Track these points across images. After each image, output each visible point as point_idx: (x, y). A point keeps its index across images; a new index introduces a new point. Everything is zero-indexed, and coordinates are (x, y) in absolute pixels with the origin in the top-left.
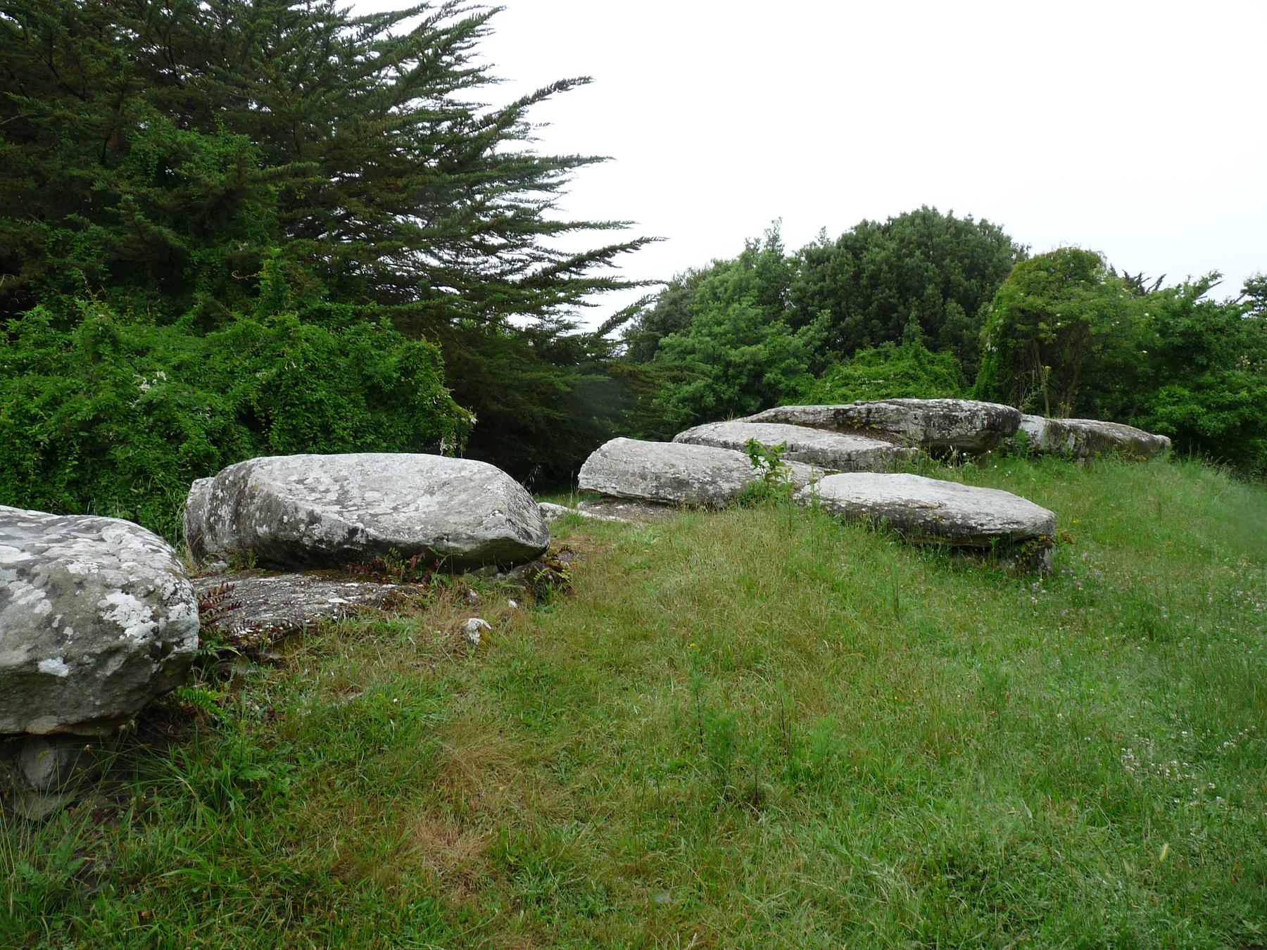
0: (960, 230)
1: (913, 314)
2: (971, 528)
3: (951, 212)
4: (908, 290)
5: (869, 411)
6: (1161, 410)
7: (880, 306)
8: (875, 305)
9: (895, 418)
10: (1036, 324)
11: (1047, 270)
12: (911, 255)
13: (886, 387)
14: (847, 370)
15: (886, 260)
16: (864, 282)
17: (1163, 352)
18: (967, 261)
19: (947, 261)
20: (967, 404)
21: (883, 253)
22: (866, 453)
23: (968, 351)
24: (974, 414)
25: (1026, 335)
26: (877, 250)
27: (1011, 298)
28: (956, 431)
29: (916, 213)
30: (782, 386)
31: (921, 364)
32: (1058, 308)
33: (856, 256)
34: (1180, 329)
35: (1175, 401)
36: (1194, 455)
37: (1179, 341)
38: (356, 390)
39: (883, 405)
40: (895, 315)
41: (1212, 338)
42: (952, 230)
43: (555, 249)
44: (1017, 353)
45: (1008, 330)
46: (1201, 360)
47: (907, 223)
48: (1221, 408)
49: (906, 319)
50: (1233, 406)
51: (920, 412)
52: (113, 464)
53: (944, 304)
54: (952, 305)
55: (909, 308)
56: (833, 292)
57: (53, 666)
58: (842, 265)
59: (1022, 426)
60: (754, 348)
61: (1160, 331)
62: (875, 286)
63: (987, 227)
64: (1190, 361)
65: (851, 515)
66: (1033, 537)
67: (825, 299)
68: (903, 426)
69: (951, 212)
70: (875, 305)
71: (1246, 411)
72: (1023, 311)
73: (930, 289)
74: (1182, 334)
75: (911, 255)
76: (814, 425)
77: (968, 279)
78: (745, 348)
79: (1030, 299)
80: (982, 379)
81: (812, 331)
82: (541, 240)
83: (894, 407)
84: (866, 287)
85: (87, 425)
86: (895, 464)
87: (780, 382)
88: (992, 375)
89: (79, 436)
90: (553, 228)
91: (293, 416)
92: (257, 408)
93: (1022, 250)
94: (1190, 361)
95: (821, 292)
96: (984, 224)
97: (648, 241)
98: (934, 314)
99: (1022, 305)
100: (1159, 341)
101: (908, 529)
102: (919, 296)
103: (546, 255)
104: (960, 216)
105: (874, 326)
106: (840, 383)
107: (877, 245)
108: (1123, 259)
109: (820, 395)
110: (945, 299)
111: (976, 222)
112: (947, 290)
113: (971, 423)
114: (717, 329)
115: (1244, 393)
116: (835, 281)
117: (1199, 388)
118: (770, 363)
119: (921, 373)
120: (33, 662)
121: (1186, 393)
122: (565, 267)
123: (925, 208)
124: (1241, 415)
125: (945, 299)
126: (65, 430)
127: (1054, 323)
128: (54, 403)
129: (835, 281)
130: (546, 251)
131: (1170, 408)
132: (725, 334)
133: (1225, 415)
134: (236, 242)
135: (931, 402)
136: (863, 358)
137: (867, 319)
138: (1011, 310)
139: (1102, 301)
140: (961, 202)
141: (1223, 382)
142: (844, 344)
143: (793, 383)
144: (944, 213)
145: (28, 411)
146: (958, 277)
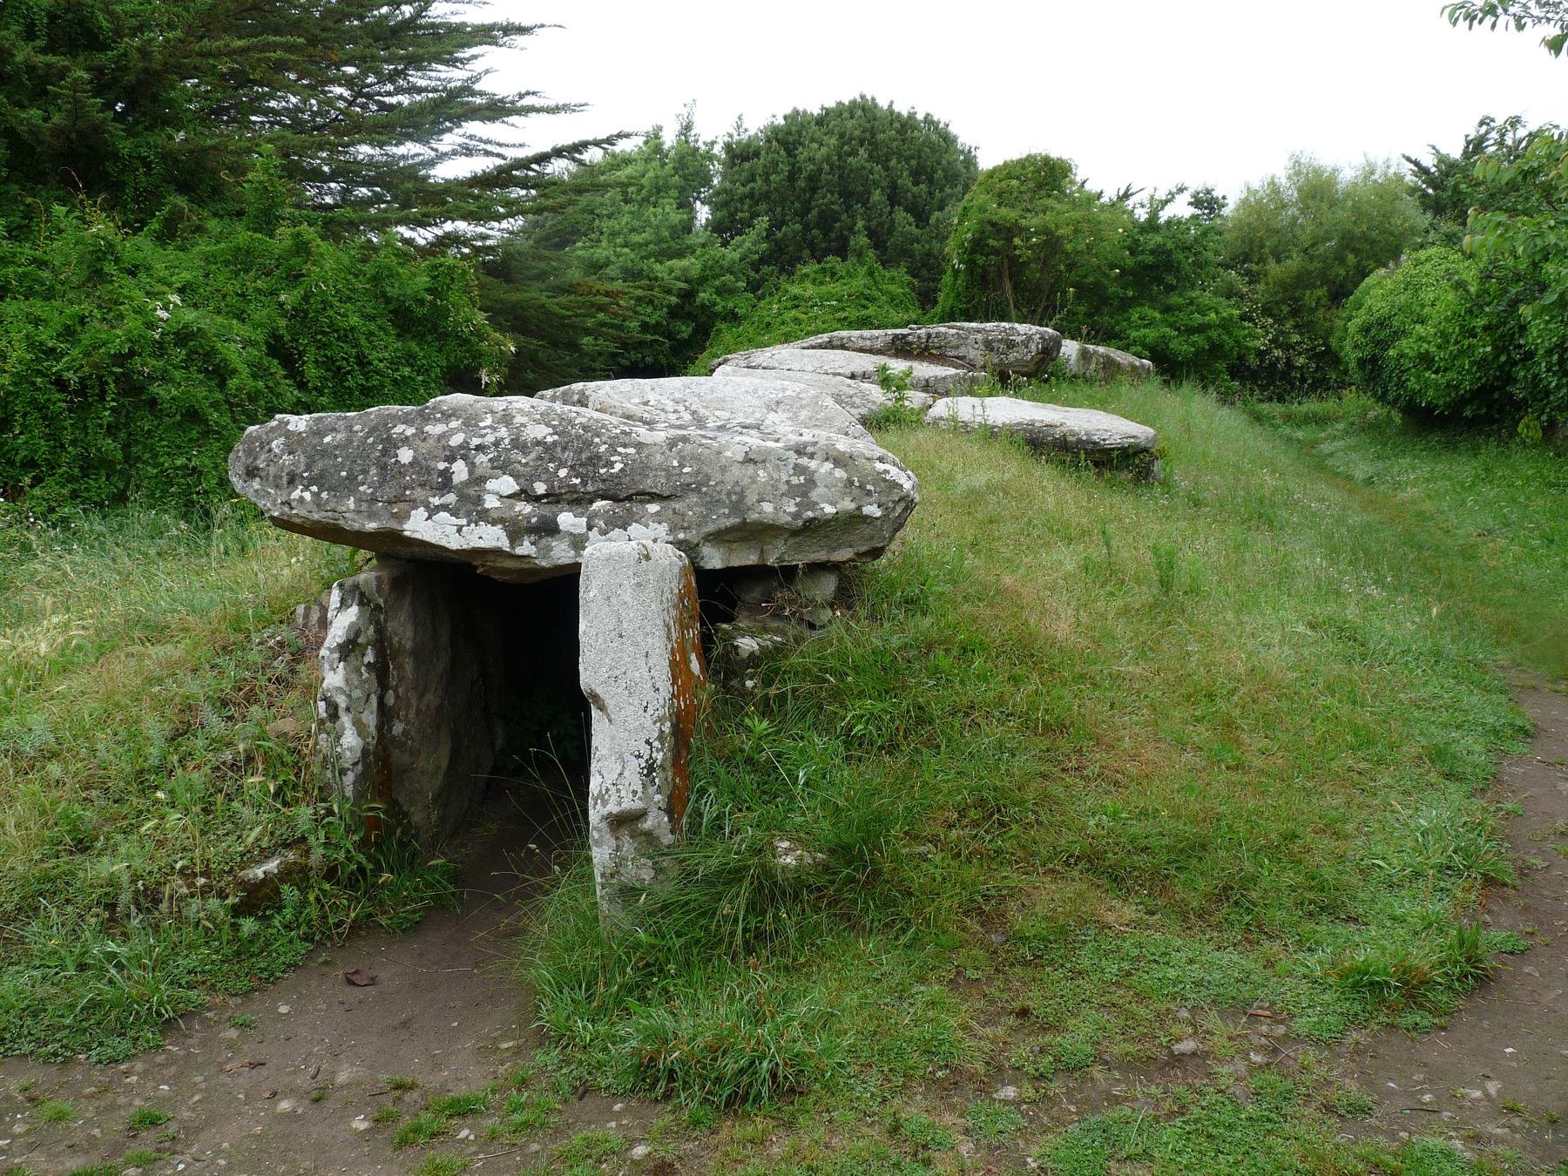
0: (905, 125)
1: (860, 224)
2: (1095, 443)
4: (851, 194)
5: (929, 336)
6: (1134, 334)
7: (820, 214)
8: (815, 212)
9: (955, 342)
10: (1010, 240)
11: (1018, 178)
12: (854, 153)
13: (843, 309)
14: (795, 290)
15: (827, 159)
16: (801, 183)
17: (1132, 272)
18: (913, 162)
19: (893, 162)
20: (1022, 328)
21: (824, 150)
22: (945, 378)
23: (926, 271)
24: (1030, 338)
25: (996, 252)
26: (815, 146)
27: (982, 209)
28: (1013, 356)
29: (853, 102)
30: (718, 308)
31: (876, 282)
32: (1033, 222)
33: (790, 153)
34: (1151, 245)
35: (1148, 324)
36: (1188, 376)
37: (1149, 259)
38: (381, 315)
39: (943, 330)
41: (1181, 256)
42: (897, 125)
43: (492, 138)
45: (978, 245)
46: (1170, 279)
47: (846, 115)
48: (1191, 331)
49: (851, 229)
50: (1201, 329)
51: (979, 336)
52: (153, 402)
54: (901, 215)
55: (852, 212)
56: (766, 196)
57: (872, 510)
58: (775, 163)
59: (1063, 349)
60: (685, 263)
61: (1129, 249)
62: (814, 190)
63: (932, 122)
64: (1159, 281)
65: (991, 434)
66: (1145, 450)
68: (962, 352)
70: (815, 212)
71: (1213, 334)
72: (993, 224)
73: (877, 196)
74: (1152, 252)
75: (854, 153)
76: (871, 351)
77: (916, 183)
78: (675, 263)
79: (1004, 211)
80: (944, 299)
81: (749, 242)
82: (474, 127)
84: (804, 190)
85: (120, 359)
86: (969, 388)
88: (959, 294)
89: (113, 373)
90: (497, 110)
91: (324, 346)
92: (287, 338)
94: (1159, 281)
95: (751, 195)
96: (928, 119)
99: (995, 218)
100: (1130, 262)
101: (1037, 443)
103: (482, 146)
104: (902, 109)
105: (814, 238)
106: (789, 304)
107: (813, 140)
108: (1101, 173)
109: (768, 319)
110: (892, 206)
111: (920, 116)
112: (894, 196)
114: (636, 238)
115: (1213, 315)
116: (767, 181)
117: (1167, 309)
118: (703, 280)
119: (877, 294)
120: (859, 508)
121: (1157, 315)
122: (524, 164)
123: (863, 97)
124: (1209, 339)
125: (892, 206)
126: (96, 366)
127: (1028, 239)
128: (68, 333)
129: (767, 181)
130: (481, 140)
131: (1144, 331)
132: (647, 244)
133: (1195, 338)
134: (170, 130)
135: (989, 326)
136: (806, 275)
137: (807, 228)
138: (981, 222)
139: (1076, 215)
140: (903, 95)
141: (1191, 303)
142: (780, 258)
143: (731, 305)
144: (883, 104)
145: (41, 344)
146: (905, 181)
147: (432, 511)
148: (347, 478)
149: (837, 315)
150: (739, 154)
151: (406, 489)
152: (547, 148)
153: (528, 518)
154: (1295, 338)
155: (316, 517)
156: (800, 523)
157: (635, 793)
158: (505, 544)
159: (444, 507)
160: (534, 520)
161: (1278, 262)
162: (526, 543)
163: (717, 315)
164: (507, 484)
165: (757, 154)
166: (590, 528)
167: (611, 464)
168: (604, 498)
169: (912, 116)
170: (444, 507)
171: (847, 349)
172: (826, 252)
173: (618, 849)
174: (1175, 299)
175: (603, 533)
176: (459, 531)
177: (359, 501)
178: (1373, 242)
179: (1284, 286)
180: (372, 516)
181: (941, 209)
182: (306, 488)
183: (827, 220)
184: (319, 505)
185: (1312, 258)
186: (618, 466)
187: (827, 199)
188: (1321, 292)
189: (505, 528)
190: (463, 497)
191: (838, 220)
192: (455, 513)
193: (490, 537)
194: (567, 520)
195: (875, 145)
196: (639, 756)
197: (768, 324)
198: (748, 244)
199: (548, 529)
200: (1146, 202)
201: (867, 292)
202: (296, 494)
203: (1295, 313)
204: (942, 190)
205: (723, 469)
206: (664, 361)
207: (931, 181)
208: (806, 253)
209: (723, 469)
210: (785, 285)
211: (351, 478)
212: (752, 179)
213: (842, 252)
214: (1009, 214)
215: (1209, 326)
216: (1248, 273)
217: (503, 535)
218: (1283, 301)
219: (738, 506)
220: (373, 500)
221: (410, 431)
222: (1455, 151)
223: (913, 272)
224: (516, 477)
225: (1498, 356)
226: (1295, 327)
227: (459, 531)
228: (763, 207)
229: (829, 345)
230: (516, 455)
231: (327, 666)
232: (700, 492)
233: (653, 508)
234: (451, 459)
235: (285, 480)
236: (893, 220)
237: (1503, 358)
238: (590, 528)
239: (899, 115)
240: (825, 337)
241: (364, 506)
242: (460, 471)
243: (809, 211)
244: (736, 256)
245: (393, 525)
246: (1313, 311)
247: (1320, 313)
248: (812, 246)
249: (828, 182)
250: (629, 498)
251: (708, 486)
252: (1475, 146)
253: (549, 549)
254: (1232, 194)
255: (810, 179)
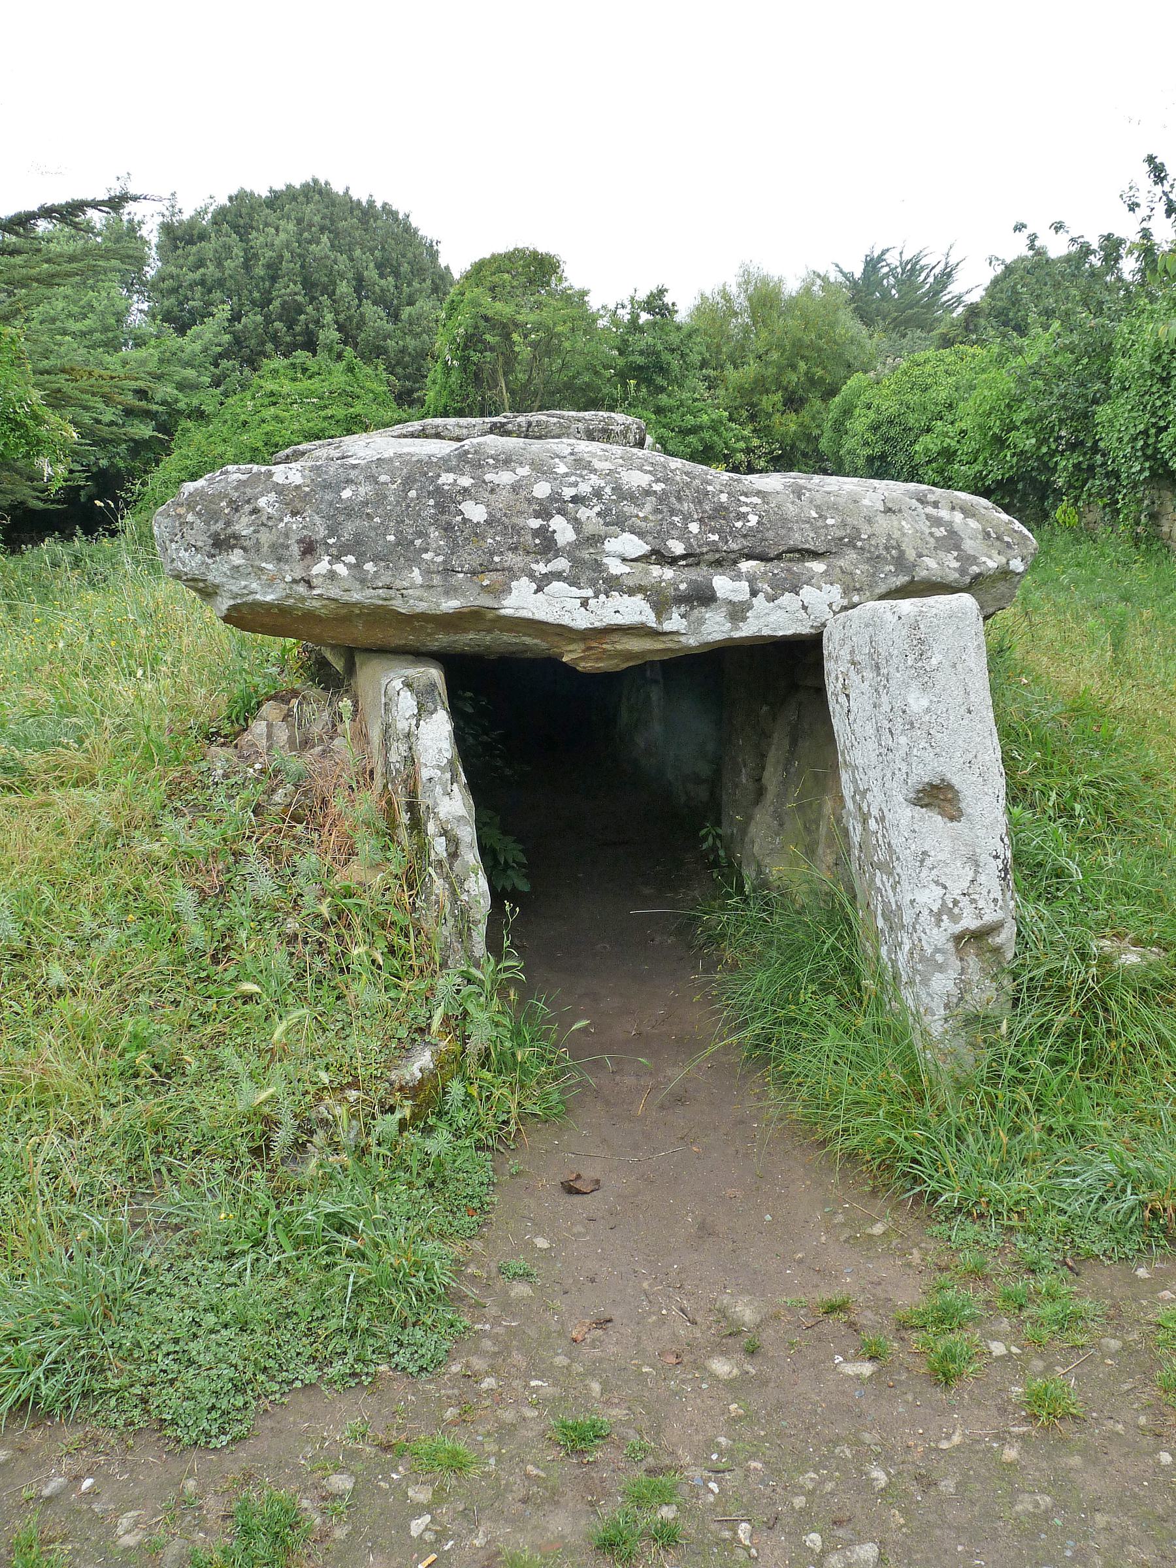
0: (366, 213)
1: (329, 317)
3: (347, 189)
4: (314, 285)
5: (530, 424)
7: (282, 306)
8: (277, 303)
14: (270, 386)
15: (287, 245)
16: (260, 271)
21: (283, 236)
30: (181, 405)
32: (528, 317)
34: (642, 345)
37: (640, 360)
39: (544, 418)
40: (303, 317)
44: (480, 370)
45: (472, 340)
46: (660, 381)
50: (694, 430)
53: (359, 306)
56: (220, 283)
62: (274, 279)
67: (210, 291)
69: (347, 189)
70: (277, 303)
71: (706, 435)
72: (486, 319)
73: (344, 288)
79: (499, 305)
81: (209, 333)
83: (555, 420)
87: (177, 401)
93: (431, 246)
95: (202, 283)
97: (888, 250)
98: (350, 318)
99: (490, 313)
102: (331, 295)
104: (360, 194)
106: (266, 401)
112: (360, 284)
113: (625, 437)
116: (219, 265)
123: (315, 181)
124: (702, 440)
127: (526, 336)
132: (91, 332)
133: (691, 439)
137: (268, 320)
141: (682, 405)
143: (195, 402)
144: (338, 188)
146: (372, 273)
147: (542, 583)
148: (398, 544)
149: (322, 413)
150: (179, 236)
151: (492, 554)
152: (34, 208)
153: (674, 584)
154: (756, 442)
155: (356, 596)
156: (968, 579)
157: (995, 900)
158: (650, 619)
159: (557, 576)
160: (683, 587)
161: (736, 367)
162: (675, 616)
163: (180, 412)
164: (635, 546)
165: (203, 237)
166: (754, 593)
167: (743, 517)
168: (749, 557)
169: (371, 203)
170: (557, 576)
171: (443, 438)
172: (294, 347)
173: (963, 971)
174: (663, 399)
175: (771, 599)
176: (585, 603)
177: (427, 573)
178: (820, 350)
179: (740, 389)
180: (450, 591)
181: (411, 303)
182: (337, 558)
183: (291, 312)
184: (363, 581)
185: (767, 364)
186: (753, 520)
187: (289, 290)
188: (778, 397)
189: (647, 598)
190: (576, 562)
191: (301, 312)
192: (574, 582)
193: (632, 610)
194: (722, 584)
195: (336, 234)
196: (997, 857)
197: (245, 423)
198: (208, 335)
199: (703, 597)
200: (626, 303)
201: (349, 389)
202: (322, 567)
203: (753, 418)
204: (409, 285)
205: (869, 520)
206: (121, 464)
207: (396, 274)
208: (269, 347)
209: (869, 520)
210: (256, 381)
211: (403, 542)
212: (200, 263)
213: (311, 345)
214: (501, 309)
215: (701, 428)
216: (706, 378)
217: (646, 607)
218: (741, 407)
219: (900, 562)
220: (448, 571)
221: (466, 481)
222: (858, 272)
223: (390, 369)
224: (641, 534)
225: (1039, 448)
226: (754, 431)
227: (585, 603)
228: (217, 295)
229: (423, 434)
230: (629, 509)
231: (438, 789)
232: (855, 547)
233: (818, 567)
234: (544, 513)
235: (295, 550)
236: (362, 315)
237: (1044, 450)
238: (754, 593)
239: (359, 202)
240: (416, 426)
241: (437, 580)
242: (563, 531)
243: (270, 302)
244: (197, 347)
245: (486, 601)
246: (769, 416)
247: (777, 417)
248: (275, 339)
249: (290, 272)
250: (779, 557)
251: (861, 539)
252: (872, 264)
253: (701, 621)
254: (684, 304)
255: (268, 266)
